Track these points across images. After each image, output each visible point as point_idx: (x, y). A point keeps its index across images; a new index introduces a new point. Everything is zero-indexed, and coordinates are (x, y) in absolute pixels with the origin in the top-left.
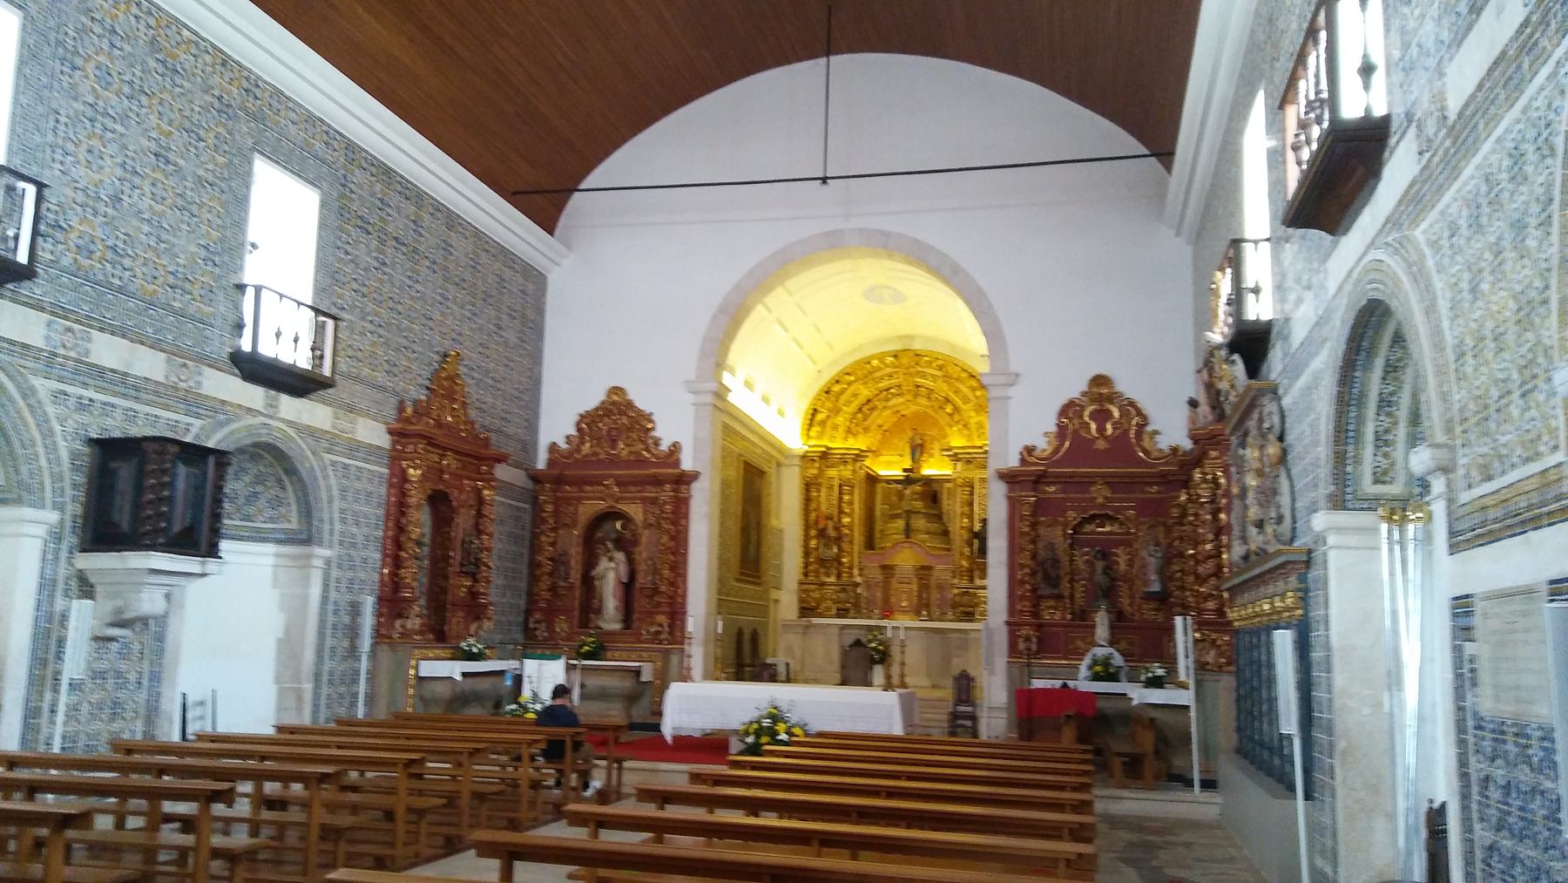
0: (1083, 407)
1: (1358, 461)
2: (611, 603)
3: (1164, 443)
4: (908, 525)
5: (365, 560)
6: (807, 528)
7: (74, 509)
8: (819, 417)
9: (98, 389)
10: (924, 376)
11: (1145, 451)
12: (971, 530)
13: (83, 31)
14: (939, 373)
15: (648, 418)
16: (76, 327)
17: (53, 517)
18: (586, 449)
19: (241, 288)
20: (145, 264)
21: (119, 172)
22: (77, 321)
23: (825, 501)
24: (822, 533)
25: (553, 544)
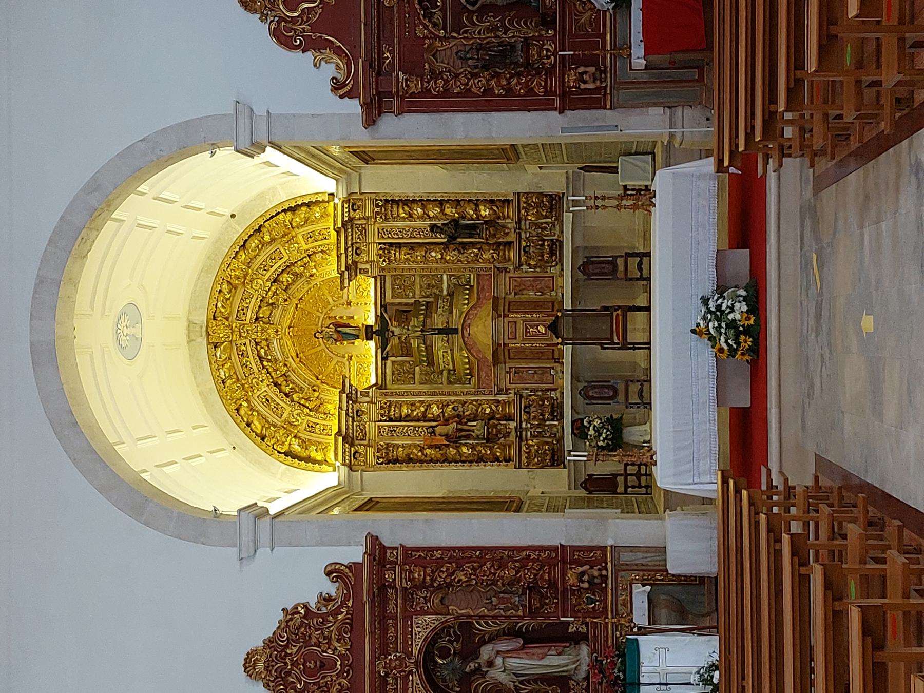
0: (282, 19)
4: (440, 331)
6: (446, 460)
8: (296, 448)
10: (242, 311)
12: (446, 246)
14: (240, 291)
15: (290, 613)
24: (454, 440)
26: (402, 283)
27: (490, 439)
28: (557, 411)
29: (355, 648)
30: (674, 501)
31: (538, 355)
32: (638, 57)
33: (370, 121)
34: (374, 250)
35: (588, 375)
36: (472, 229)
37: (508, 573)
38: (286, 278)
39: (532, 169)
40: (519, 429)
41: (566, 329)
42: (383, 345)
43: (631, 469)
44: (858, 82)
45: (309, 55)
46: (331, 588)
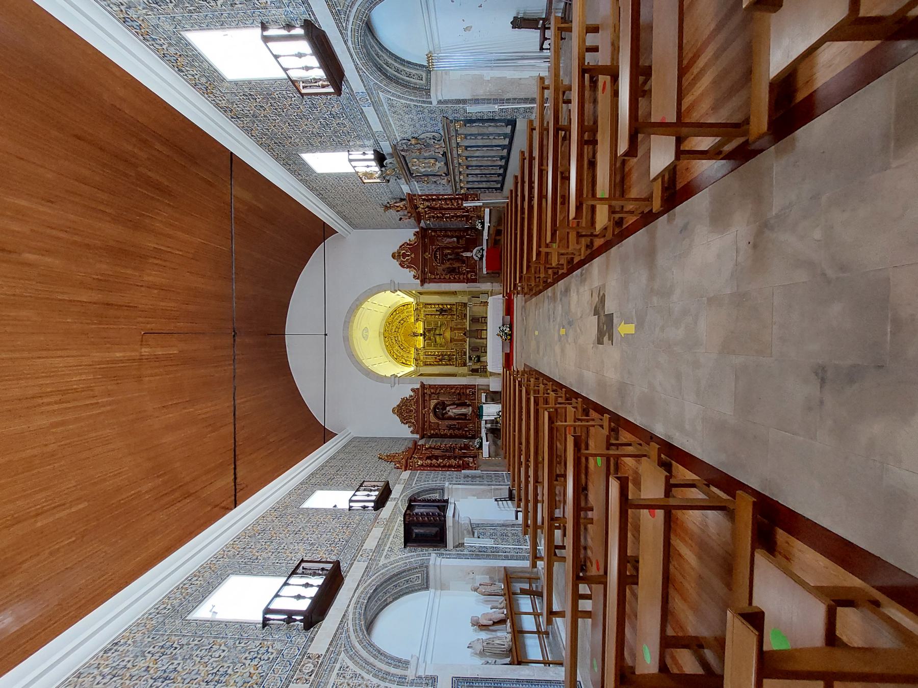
1: (415, 84)
2: (463, 410)
3: (413, 238)
5: (450, 475)
7: (430, 550)
8: (404, 362)
9: (385, 545)
10: (392, 329)
11: (415, 243)
12: (439, 315)
13: (242, 557)
16: (360, 553)
17: (433, 555)
18: (413, 421)
19: (350, 508)
20: (338, 535)
21: (301, 544)
22: (359, 553)
23: (430, 360)
24: (441, 360)
25: (444, 430)
26: (429, 323)
27: (449, 360)
28: (465, 354)
29: (418, 407)
30: (492, 374)
31: (461, 340)
32: (485, 271)
33: (422, 285)
34: (423, 315)
35: (472, 345)
36: (445, 311)
37: (453, 391)
38: (402, 322)
39: (460, 297)
40: (456, 358)
41: (468, 334)
42: (424, 338)
43: (482, 367)
44: (535, 277)
45: (408, 269)
46: (412, 394)
